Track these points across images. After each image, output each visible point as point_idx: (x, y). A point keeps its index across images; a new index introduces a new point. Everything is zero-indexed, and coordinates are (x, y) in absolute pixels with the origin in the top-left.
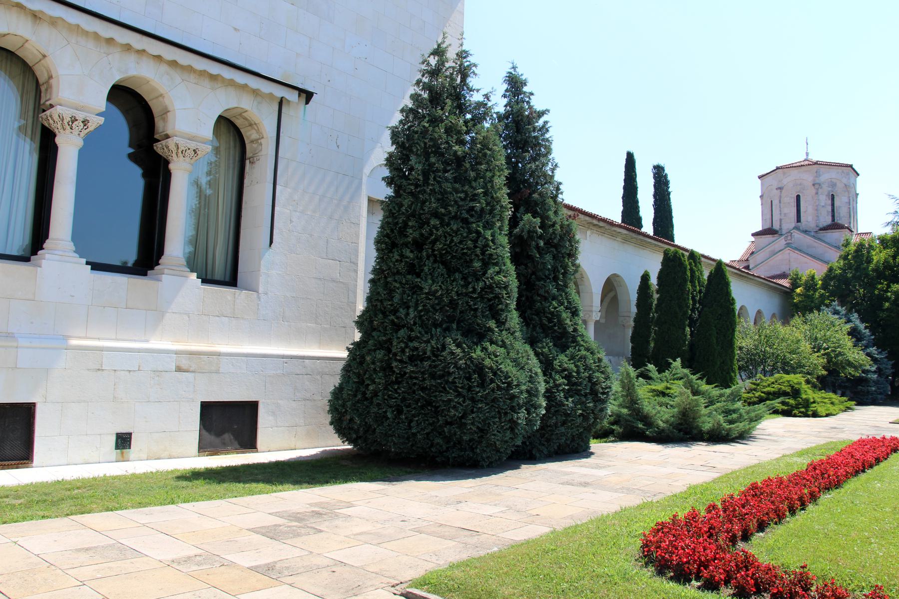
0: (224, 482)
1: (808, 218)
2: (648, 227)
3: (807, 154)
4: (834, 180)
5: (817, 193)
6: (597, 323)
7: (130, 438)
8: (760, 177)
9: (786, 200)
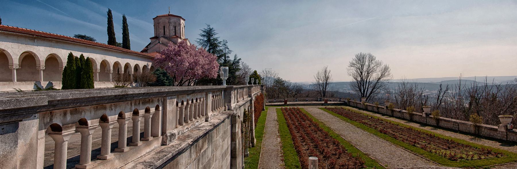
1: (167, 34)
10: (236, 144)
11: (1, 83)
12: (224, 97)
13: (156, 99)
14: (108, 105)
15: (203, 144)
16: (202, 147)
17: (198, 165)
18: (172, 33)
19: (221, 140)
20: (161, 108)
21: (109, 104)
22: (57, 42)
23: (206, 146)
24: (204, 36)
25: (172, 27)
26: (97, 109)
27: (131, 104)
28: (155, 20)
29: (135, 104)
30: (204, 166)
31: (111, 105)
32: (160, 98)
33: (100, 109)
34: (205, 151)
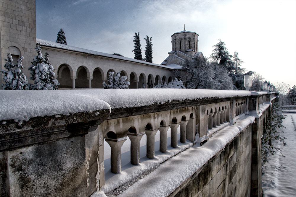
0: (218, 103)
1: (183, 48)
2: (144, 56)
3: (185, 29)
4: (190, 37)
5: (185, 41)
6: (75, 79)
7: (182, 119)
8: (171, 36)
9: (177, 43)
10: (257, 150)
11: (190, 196)
12: (249, 104)
13: (190, 108)
14: (152, 114)
15: (230, 150)
16: (230, 153)
17: (226, 170)
18: (187, 46)
19: (244, 147)
20: (194, 116)
21: (153, 113)
22: (101, 59)
23: (232, 153)
24: (216, 50)
25: (187, 43)
26: (143, 118)
27: (171, 113)
28: (173, 36)
29: (174, 113)
30: (231, 171)
31: (154, 114)
32: (194, 107)
33: (145, 118)
34: (232, 157)
